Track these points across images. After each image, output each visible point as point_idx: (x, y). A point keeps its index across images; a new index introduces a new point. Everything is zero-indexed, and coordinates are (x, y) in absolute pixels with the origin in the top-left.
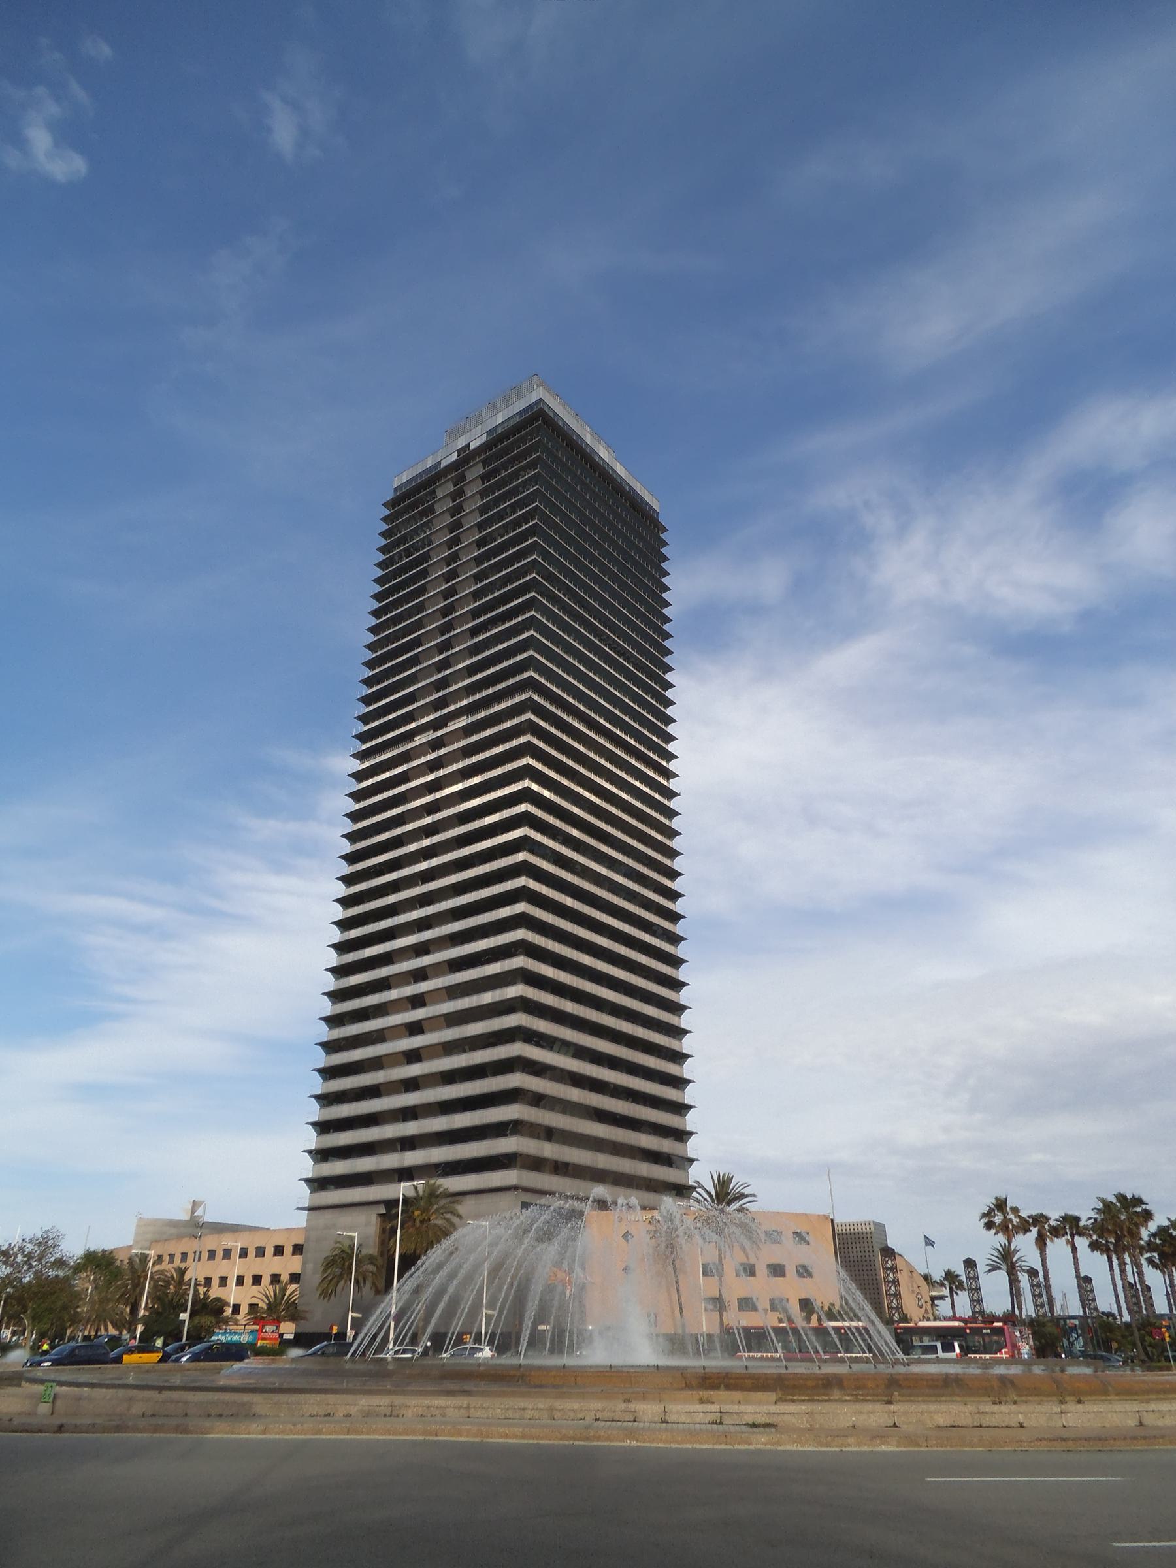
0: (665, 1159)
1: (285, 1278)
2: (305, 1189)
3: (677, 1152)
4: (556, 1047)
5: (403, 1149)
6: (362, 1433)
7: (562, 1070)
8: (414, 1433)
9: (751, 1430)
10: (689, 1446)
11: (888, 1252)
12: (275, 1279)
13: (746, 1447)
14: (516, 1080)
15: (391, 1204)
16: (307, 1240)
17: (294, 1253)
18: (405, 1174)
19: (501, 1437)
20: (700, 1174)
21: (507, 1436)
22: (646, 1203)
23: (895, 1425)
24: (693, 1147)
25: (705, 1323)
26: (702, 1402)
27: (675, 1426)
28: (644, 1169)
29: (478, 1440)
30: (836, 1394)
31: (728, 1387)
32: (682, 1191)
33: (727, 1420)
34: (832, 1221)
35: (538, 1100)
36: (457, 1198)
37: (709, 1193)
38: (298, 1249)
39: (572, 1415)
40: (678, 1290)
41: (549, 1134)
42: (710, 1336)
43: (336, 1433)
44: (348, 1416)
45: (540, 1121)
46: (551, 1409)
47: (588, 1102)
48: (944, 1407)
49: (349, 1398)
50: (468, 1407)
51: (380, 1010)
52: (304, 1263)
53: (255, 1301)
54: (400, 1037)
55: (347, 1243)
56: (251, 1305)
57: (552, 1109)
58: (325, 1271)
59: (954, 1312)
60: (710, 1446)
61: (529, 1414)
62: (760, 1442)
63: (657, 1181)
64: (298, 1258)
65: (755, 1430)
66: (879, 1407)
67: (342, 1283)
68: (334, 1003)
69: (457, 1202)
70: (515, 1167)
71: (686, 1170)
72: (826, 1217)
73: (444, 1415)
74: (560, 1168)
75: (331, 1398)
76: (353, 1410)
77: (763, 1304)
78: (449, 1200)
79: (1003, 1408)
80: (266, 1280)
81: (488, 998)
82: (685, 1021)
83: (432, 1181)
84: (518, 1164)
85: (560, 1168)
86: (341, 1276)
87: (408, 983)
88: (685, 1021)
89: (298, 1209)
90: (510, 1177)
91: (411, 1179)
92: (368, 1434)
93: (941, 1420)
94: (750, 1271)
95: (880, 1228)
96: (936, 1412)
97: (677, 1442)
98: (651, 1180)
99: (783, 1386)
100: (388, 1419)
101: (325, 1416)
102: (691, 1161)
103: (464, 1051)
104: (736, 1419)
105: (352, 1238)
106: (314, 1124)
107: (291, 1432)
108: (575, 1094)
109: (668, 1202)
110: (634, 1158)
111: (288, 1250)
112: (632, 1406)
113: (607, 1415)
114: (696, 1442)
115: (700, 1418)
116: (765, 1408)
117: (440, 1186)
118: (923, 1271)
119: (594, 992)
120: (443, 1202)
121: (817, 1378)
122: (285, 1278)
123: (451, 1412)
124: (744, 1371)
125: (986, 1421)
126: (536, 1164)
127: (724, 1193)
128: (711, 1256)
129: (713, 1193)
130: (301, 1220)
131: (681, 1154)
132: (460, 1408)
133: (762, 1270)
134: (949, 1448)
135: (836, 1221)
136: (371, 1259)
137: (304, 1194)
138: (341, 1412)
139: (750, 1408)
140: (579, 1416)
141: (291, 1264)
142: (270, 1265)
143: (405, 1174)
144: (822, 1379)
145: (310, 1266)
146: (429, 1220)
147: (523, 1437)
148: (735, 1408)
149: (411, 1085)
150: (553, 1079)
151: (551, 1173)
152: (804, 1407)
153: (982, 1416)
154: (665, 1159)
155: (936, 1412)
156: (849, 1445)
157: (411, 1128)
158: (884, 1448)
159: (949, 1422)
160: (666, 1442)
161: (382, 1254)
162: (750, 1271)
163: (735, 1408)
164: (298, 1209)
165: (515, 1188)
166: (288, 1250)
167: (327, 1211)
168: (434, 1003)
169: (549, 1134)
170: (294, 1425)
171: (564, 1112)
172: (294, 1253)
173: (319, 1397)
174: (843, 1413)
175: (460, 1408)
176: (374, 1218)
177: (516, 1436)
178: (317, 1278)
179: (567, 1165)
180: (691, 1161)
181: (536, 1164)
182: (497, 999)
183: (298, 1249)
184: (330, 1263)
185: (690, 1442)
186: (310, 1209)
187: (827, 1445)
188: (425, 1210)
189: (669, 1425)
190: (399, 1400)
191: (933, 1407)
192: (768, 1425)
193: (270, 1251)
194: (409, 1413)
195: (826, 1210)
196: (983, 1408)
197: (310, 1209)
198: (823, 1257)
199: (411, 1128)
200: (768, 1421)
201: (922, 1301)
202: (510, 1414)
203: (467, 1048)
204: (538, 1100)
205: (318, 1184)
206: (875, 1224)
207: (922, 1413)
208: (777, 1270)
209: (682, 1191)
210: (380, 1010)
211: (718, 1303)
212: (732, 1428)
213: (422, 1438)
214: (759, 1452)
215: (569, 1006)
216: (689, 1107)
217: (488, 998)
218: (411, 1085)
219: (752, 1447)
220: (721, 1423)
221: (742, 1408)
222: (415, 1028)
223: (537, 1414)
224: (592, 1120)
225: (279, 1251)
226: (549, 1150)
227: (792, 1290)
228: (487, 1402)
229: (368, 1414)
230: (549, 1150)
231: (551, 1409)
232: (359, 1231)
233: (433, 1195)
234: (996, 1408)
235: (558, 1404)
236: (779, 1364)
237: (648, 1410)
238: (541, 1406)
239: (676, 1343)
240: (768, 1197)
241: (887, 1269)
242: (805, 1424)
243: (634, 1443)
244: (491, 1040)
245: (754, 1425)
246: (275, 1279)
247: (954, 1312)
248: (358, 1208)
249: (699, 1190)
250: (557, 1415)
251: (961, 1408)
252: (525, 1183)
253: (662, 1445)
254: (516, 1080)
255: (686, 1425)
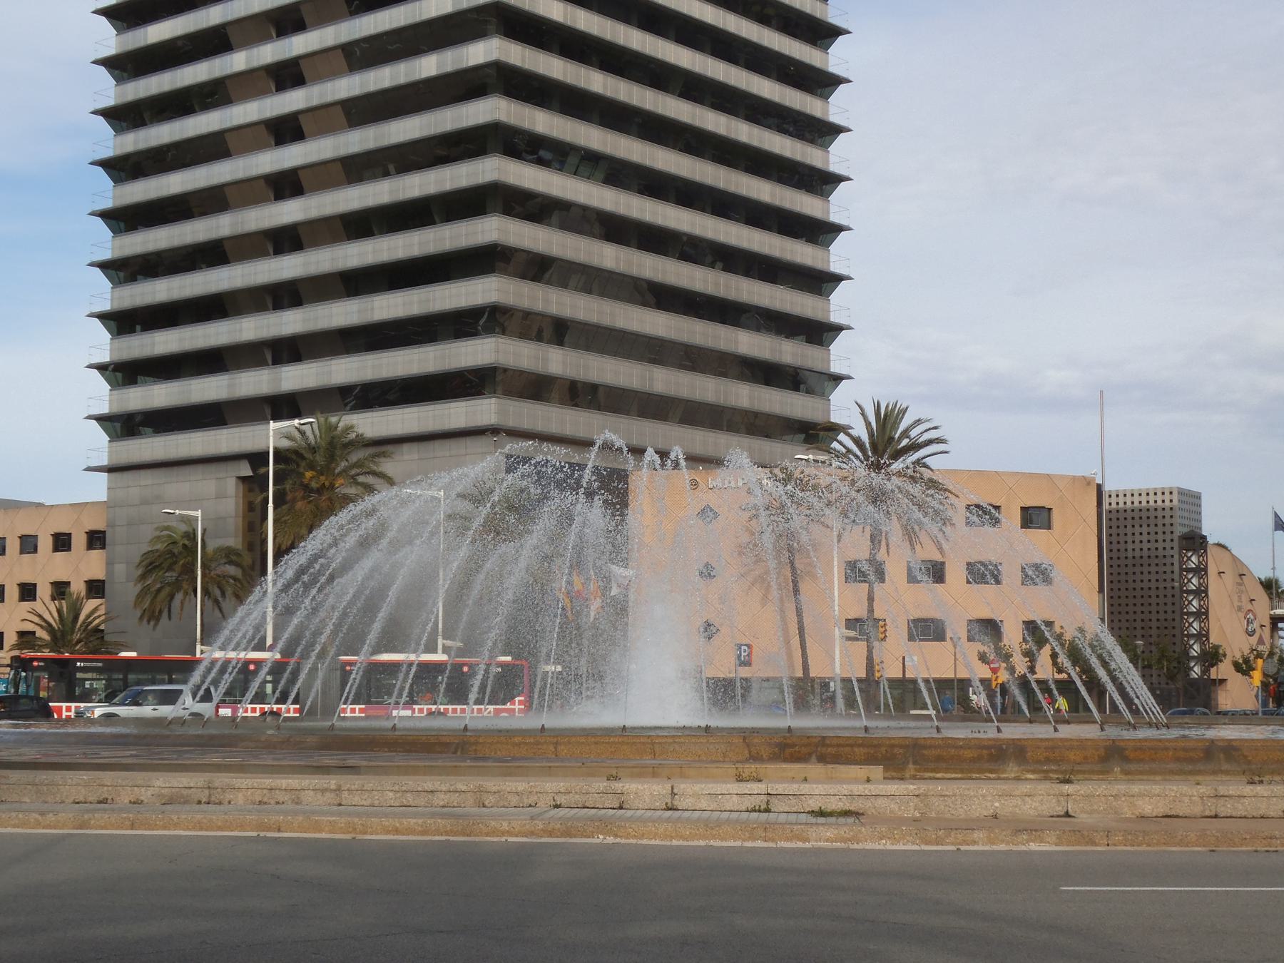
0: (791, 378)
1: (78, 587)
2: (99, 436)
3: (809, 364)
4: (573, 160)
5: (277, 361)
6: (156, 827)
7: (585, 209)
8: (242, 827)
9: (813, 820)
10: (702, 843)
11: (1195, 541)
12: (60, 589)
13: (800, 845)
14: (489, 229)
15: (258, 459)
16: (111, 524)
17: (90, 546)
18: (284, 406)
19: (388, 832)
20: (846, 408)
21: (397, 831)
22: (699, 450)
23: (1067, 815)
24: (839, 356)
25: (839, 660)
26: (740, 779)
27: (687, 814)
28: (744, 395)
29: (348, 836)
30: (1012, 769)
31: (823, 759)
32: (816, 434)
33: (777, 805)
34: (1099, 487)
35: (538, 268)
36: (384, 448)
37: (857, 441)
38: (96, 539)
39: (514, 800)
40: (797, 602)
41: (559, 331)
42: (846, 681)
43: (113, 827)
44: (137, 802)
45: (539, 307)
46: (480, 791)
47: (635, 271)
48: (1157, 789)
49: (139, 776)
50: (338, 790)
51: (213, 94)
52: (110, 563)
53: (29, 627)
54: (256, 146)
55: (184, 528)
56: (22, 634)
57: (563, 284)
58: (143, 577)
59: (871, 610)
60: (738, 843)
61: (441, 799)
62: (824, 837)
63: (769, 417)
64: (96, 554)
65: (821, 820)
66: (1044, 787)
67: (179, 597)
68: (119, 80)
69: (384, 454)
70: (494, 392)
71: (825, 396)
72: (1087, 481)
73: (297, 802)
74: (580, 394)
75: (107, 777)
76: (145, 794)
77: (957, 628)
78: (371, 451)
79: (1259, 788)
80: (44, 591)
81: (429, 66)
82: (836, 108)
83: (334, 419)
84: (500, 389)
85: (580, 394)
86: (177, 586)
87: (264, 38)
88: (836, 108)
89: (89, 469)
90: (484, 410)
91: (297, 414)
92: (165, 828)
93: (1147, 808)
94: (937, 573)
95: (1192, 500)
96: (1141, 795)
97: (682, 838)
98: (756, 414)
99: (897, 759)
100: (204, 807)
101: (100, 802)
102: (837, 379)
103: (386, 174)
104: (794, 804)
105: (190, 521)
106: (103, 317)
107: (38, 824)
108: (608, 256)
109: (802, 457)
110: (723, 374)
111: (79, 541)
112: (618, 786)
113: (579, 799)
114: (714, 837)
115: (733, 803)
116: (845, 788)
117: (349, 428)
118: (1265, 574)
119: (786, 51)
120: (355, 457)
121: (980, 745)
122: (78, 587)
123: (308, 796)
124: (862, 734)
125: (1226, 808)
126: (536, 387)
127: (887, 440)
128: (858, 547)
129: (865, 438)
130: (97, 489)
131: (819, 367)
132: (324, 791)
133: (956, 573)
134: (1144, 848)
135: (1106, 488)
136: (229, 555)
137: (99, 445)
138: (125, 798)
139: (818, 789)
140: (526, 802)
141: (84, 566)
142: (47, 568)
143: (284, 406)
144: (988, 748)
145: (120, 569)
146: (332, 487)
147: (424, 833)
148: (794, 788)
149: (286, 240)
150: (565, 226)
151: (562, 402)
152: (912, 787)
153: (1222, 801)
154: (791, 378)
155: (1141, 795)
156: (975, 843)
157: (290, 322)
158: (1034, 847)
159: (1161, 810)
160: (666, 837)
161: (250, 547)
162: (937, 573)
163: (794, 788)
164: (89, 469)
165: (494, 431)
166: (79, 541)
167: (142, 473)
168: (321, 77)
169: (559, 331)
170: (42, 814)
171: (587, 289)
172: (90, 546)
173: (84, 776)
174: (980, 797)
175: (324, 791)
176: (231, 486)
177: (410, 831)
178: (133, 590)
179: (594, 388)
180: (837, 379)
181: (536, 387)
182: (449, 68)
183: (96, 539)
184: (152, 565)
185: (704, 837)
186: (111, 470)
187: (938, 842)
188: (326, 470)
189: (677, 814)
190: (221, 779)
191: (1136, 788)
192: (846, 813)
193: (45, 543)
194: (240, 798)
195: (1089, 468)
196: (1222, 790)
197: (111, 470)
198: (1074, 554)
199: (290, 322)
200: (848, 807)
201: (1256, 625)
202: (410, 798)
203: (391, 168)
204: (538, 268)
205: (123, 425)
206: (1182, 492)
207: (1115, 796)
208: (982, 573)
209: (816, 434)
210: (213, 94)
211: (863, 627)
212: (783, 817)
213: (254, 834)
214: (817, 852)
215: (597, 82)
216: (837, 279)
217: (429, 66)
218: (286, 240)
219: (807, 845)
220: (767, 810)
221: (805, 788)
222: (286, 130)
223: (455, 799)
224: (645, 304)
225: (62, 542)
226: (558, 361)
227: (1012, 607)
228: (370, 782)
229: (171, 800)
230: (558, 361)
231: (480, 791)
232: (205, 506)
233: (336, 446)
234: (1248, 790)
235: (491, 784)
236: (928, 724)
237: (645, 792)
238: (461, 787)
239: (724, 692)
240: (970, 445)
241: (1189, 570)
242: (911, 812)
243: (610, 840)
244: (441, 152)
245: (821, 813)
246: (60, 589)
247: (871, 610)
248: (200, 468)
249: (842, 437)
250: (489, 800)
251: (1185, 788)
252: (511, 423)
253: (658, 842)
254: (489, 229)
255: (713, 811)
